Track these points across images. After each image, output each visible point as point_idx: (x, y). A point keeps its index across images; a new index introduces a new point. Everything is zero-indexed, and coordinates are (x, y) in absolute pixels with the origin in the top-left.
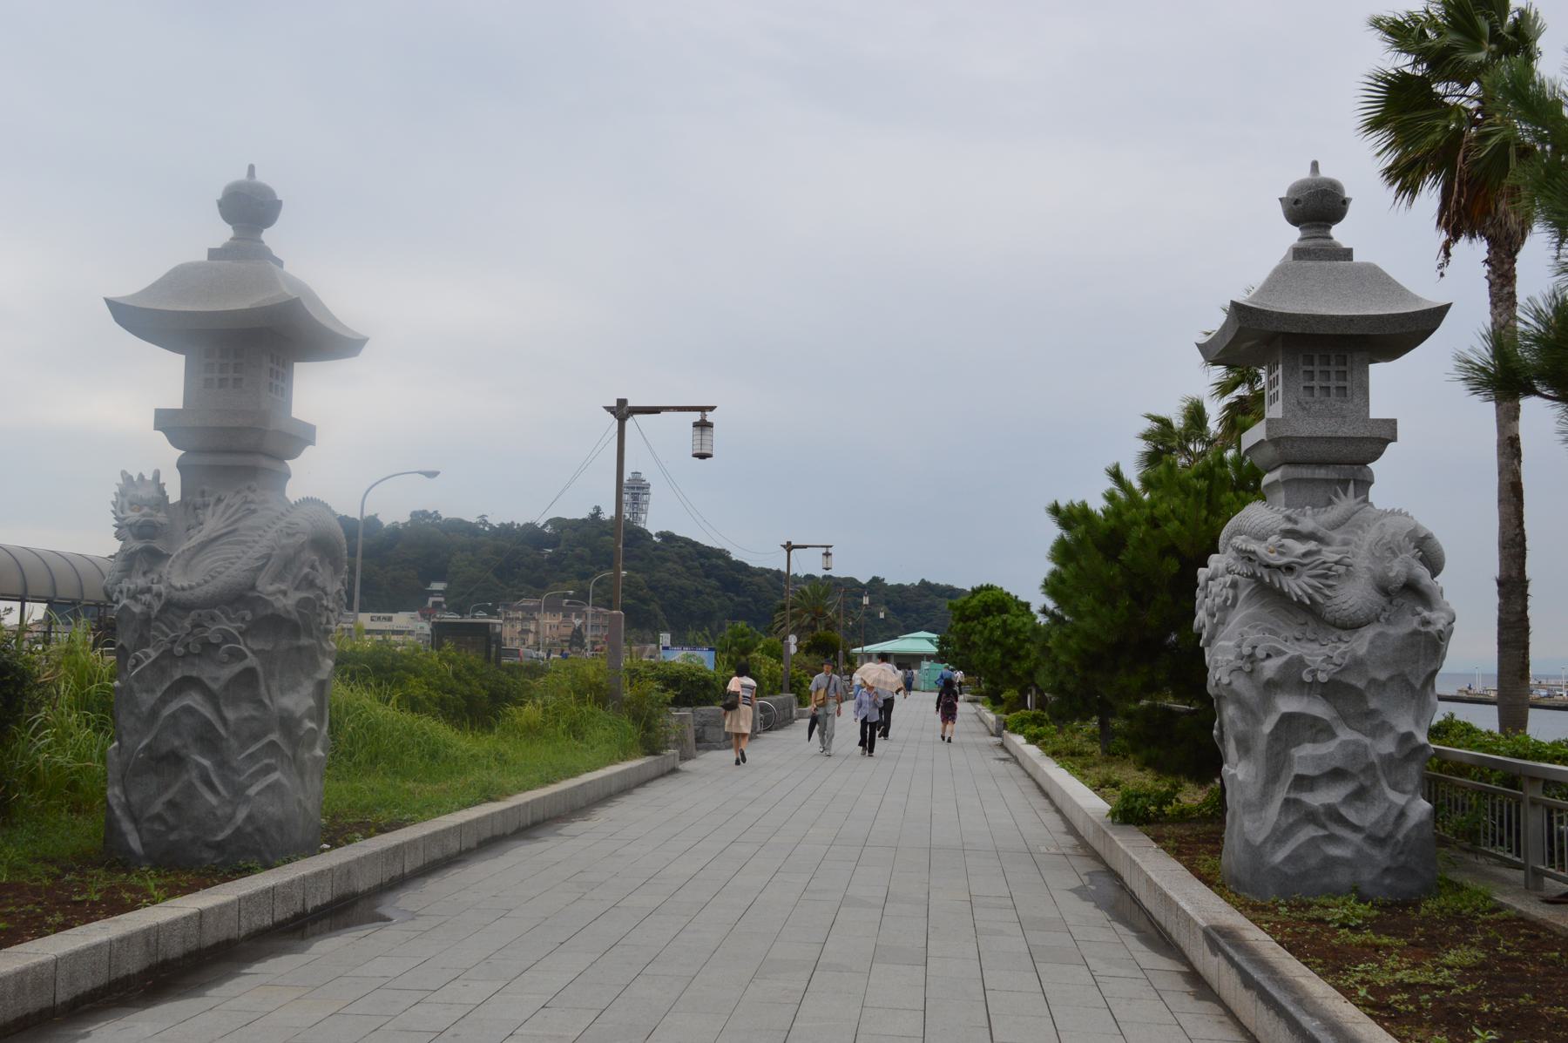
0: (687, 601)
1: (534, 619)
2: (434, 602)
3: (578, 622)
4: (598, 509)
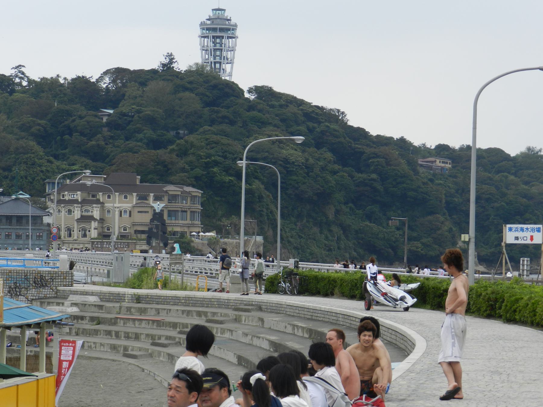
0: (294, 177)
1: (98, 202)
3: (158, 206)
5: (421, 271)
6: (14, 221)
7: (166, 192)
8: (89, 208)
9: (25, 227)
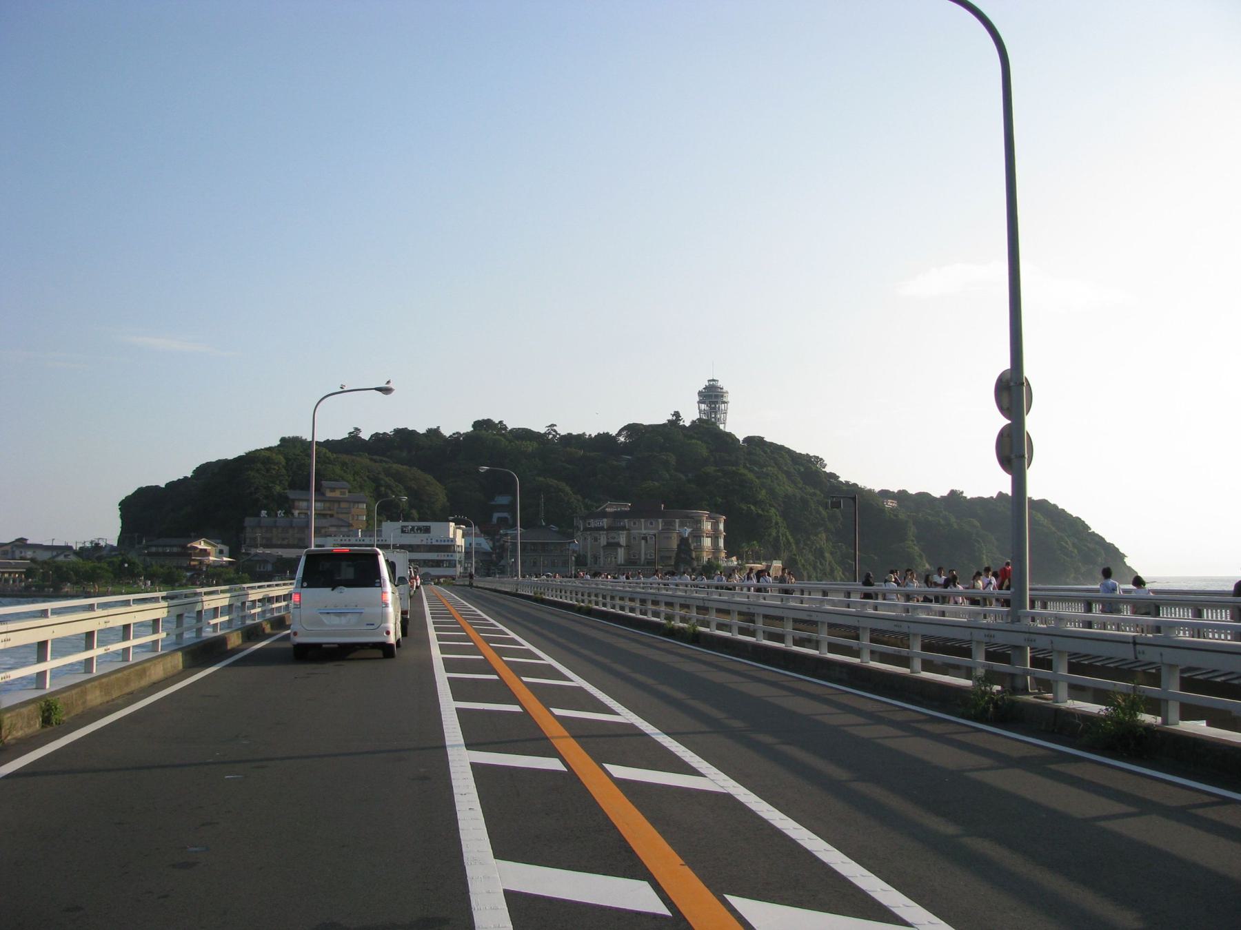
4: (677, 414)
5: (761, 579)
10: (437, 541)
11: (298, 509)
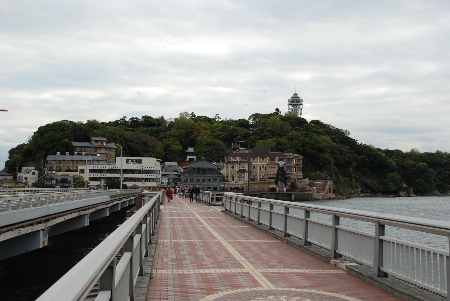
2: (190, 159)
3: (281, 164)
6: (201, 172)
7: (285, 156)
8: (244, 165)
9: (207, 175)
10: (146, 168)
11: (77, 151)
